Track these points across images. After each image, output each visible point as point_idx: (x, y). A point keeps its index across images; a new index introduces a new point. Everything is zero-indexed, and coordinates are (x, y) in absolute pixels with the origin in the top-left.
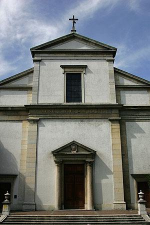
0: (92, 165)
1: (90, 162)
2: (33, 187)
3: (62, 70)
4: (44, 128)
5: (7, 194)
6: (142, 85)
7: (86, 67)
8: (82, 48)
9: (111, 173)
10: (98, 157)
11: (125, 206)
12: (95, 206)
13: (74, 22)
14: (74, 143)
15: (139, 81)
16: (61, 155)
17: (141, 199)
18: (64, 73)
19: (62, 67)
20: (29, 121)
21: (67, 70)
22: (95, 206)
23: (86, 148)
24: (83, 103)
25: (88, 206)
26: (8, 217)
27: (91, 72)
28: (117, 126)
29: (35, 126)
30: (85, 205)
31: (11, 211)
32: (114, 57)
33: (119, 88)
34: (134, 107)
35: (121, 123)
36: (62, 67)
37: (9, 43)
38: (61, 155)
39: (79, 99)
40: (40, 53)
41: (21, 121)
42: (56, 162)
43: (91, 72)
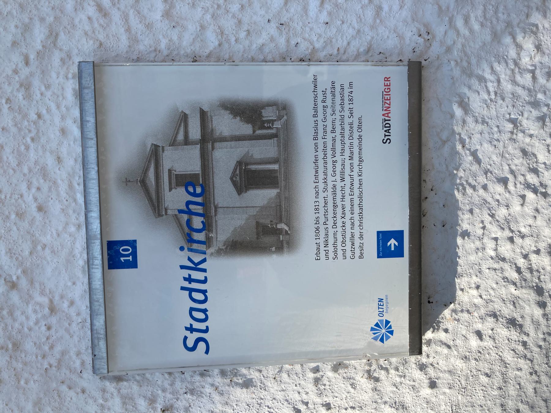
0: (247, 164)
1: (245, 166)
2: (258, 209)
3: (173, 190)
4: (236, 195)
5: (270, 226)
6: (182, 124)
7: (170, 171)
8: (154, 183)
9: (248, 152)
10: (243, 157)
11: (275, 139)
12: (275, 161)
13: (129, 181)
14: (231, 179)
15: (180, 126)
16: (241, 187)
17: (270, 125)
18: (176, 189)
19: (170, 190)
20: (215, 215)
21: (173, 185)
22: (275, 161)
23: (235, 170)
24: (200, 172)
25: (276, 167)
26: (285, 224)
27: (173, 166)
28: (217, 145)
29: (220, 211)
30: (276, 169)
31: (281, 221)
32: (159, 146)
33: (187, 142)
34: (201, 131)
35: (215, 141)
36: (170, 190)
37: (49, 270)
38: (241, 187)
39: (196, 175)
40: (159, 210)
41: (216, 221)
42: (246, 192)
43: (173, 166)
